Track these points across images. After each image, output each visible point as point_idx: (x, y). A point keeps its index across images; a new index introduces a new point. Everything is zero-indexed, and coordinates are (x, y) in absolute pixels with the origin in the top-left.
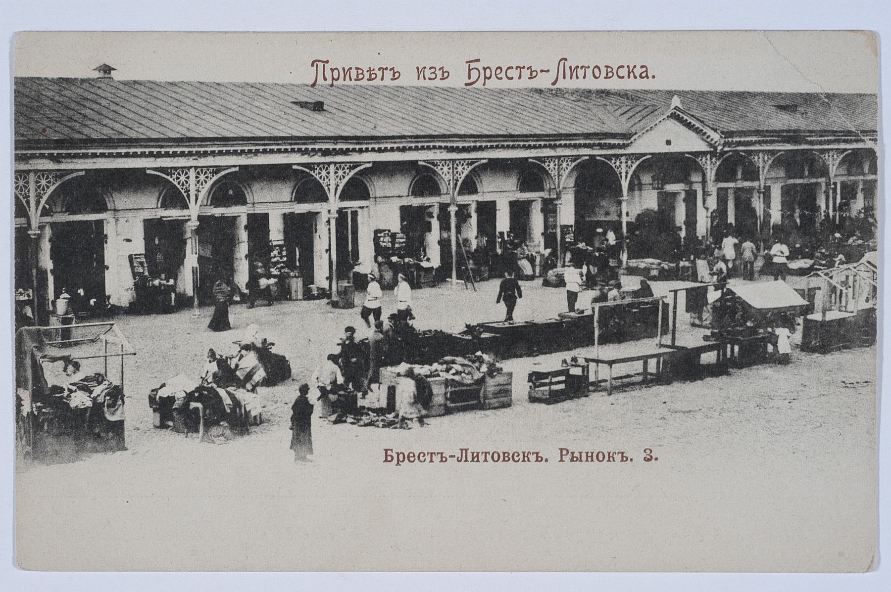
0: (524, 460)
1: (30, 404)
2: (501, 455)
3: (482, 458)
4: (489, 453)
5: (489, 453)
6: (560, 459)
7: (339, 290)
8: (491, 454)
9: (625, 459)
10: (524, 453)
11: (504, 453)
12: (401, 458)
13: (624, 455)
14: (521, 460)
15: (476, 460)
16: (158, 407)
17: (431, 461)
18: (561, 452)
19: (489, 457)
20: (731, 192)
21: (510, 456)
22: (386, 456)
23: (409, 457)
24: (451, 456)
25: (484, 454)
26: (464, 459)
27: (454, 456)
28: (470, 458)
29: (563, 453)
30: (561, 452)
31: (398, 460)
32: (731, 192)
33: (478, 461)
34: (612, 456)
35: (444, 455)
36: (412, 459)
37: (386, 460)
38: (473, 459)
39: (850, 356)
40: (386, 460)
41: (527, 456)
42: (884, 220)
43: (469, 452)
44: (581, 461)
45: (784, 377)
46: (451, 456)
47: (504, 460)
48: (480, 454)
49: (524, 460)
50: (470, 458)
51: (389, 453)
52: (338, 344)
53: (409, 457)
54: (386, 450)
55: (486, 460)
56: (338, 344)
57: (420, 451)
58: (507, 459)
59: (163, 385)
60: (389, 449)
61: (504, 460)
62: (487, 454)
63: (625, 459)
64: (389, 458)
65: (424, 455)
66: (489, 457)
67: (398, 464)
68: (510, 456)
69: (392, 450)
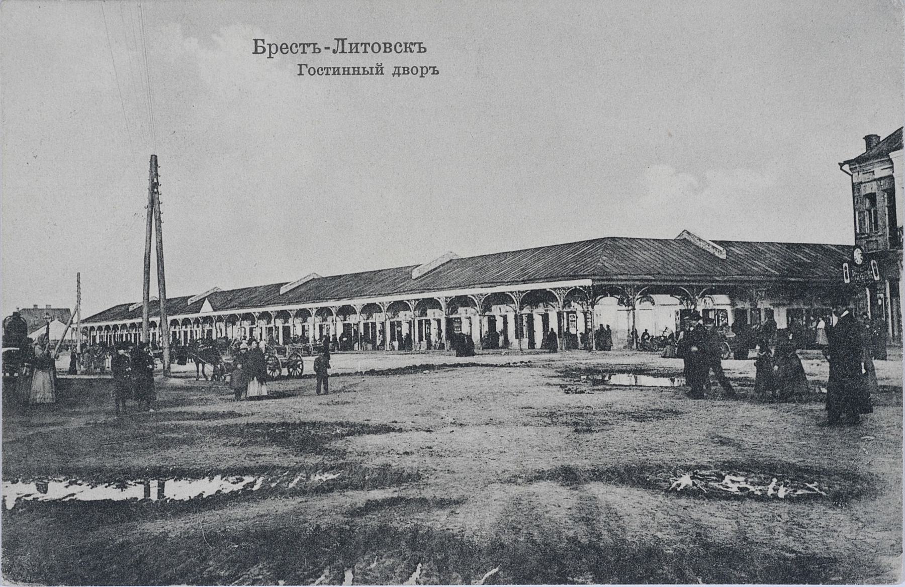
0: (406, 51)
4: (369, 44)
5: (369, 44)
6: (302, 51)
8: (371, 45)
10: (406, 44)
11: (385, 44)
12: (273, 50)
14: (404, 50)
17: (304, 52)
18: (256, 43)
19: (369, 49)
20: (424, 321)
23: (281, 48)
24: (326, 48)
25: (363, 45)
26: (340, 50)
28: (347, 48)
30: (256, 43)
32: (424, 321)
34: (409, 47)
36: (285, 51)
37: (256, 52)
40: (256, 52)
42: (150, 492)
43: (346, 42)
46: (326, 48)
47: (385, 51)
49: (406, 51)
50: (347, 48)
51: (260, 43)
52: (190, 497)
53: (281, 48)
54: (256, 41)
55: (365, 52)
56: (190, 497)
59: (67, 487)
61: (385, 51)
62: (367, 45)
64: (260, 50)
65: (296, 47)
66: (369, 49)
69: (263, 40)
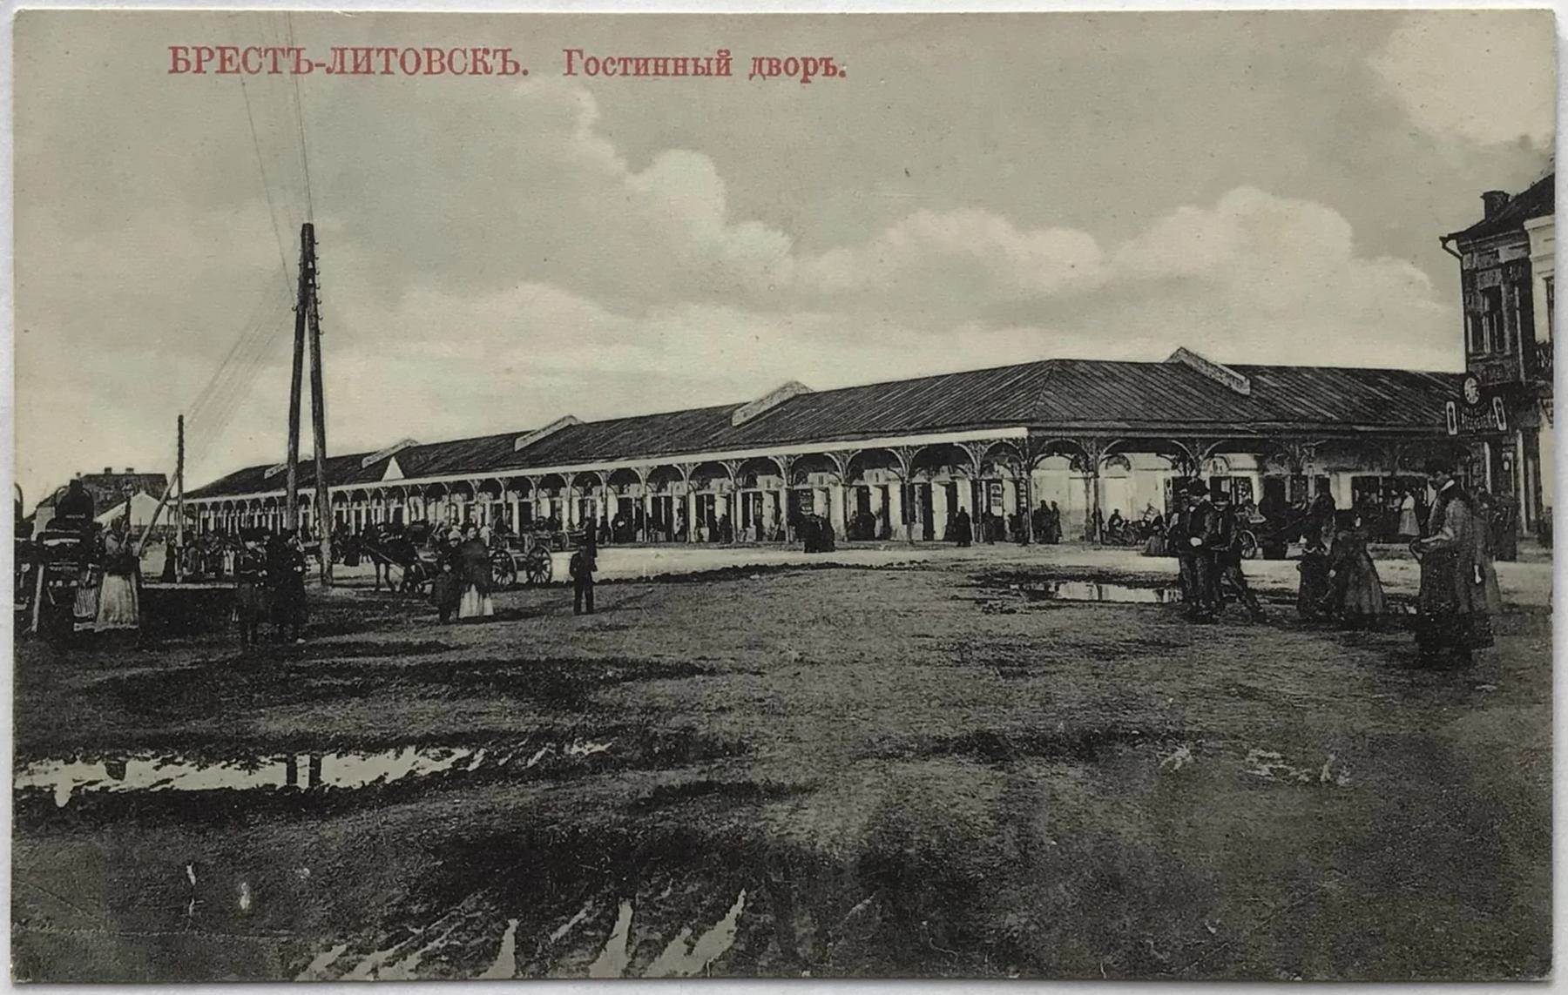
1: (24, 499)
2: (801, 63)
3: (378, 62)
5: (395, 51)
7: (1465, 268)
9: (831, 71)
13: (831, 63)
15: (723, 72)
16: (514, 923)
19: (395, 62)
21: (782, 66)
22: (176, 59)
27: (323, 65)
29: (433, 58)
31: (806, 73)
33: (685, 73)
35: (510, 56)
37: (175, 70)
38: (719, 69)
39: (331, 406)
40: (175, 70)
41: (482, 60)
44: (709, 74)
45: (1386, 751)
48: (374, 53)
51: (181, 54)
54: (175, 50)
57: (248, 46)
58: (775, 71)
60: (181, 48)
61: (430, 71)
62: (391, 53)
63: (831, 71)
66: (395, 62)
67: (805, 80)
68: (782, 66)
